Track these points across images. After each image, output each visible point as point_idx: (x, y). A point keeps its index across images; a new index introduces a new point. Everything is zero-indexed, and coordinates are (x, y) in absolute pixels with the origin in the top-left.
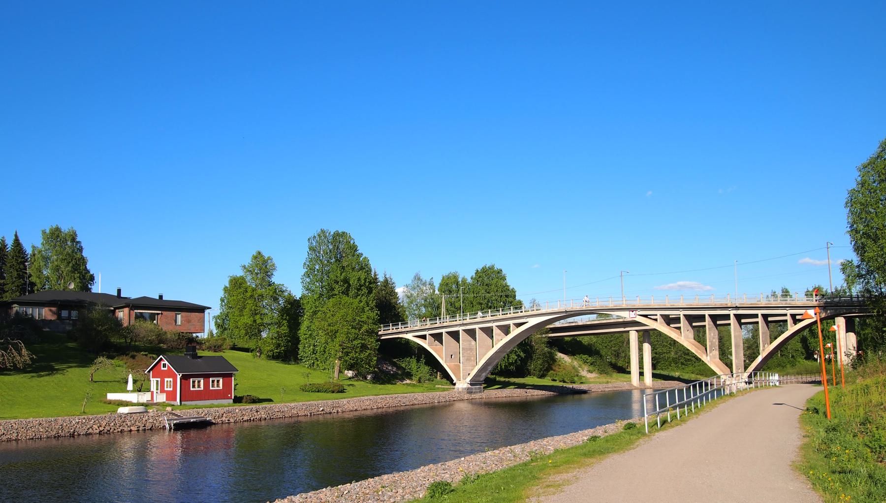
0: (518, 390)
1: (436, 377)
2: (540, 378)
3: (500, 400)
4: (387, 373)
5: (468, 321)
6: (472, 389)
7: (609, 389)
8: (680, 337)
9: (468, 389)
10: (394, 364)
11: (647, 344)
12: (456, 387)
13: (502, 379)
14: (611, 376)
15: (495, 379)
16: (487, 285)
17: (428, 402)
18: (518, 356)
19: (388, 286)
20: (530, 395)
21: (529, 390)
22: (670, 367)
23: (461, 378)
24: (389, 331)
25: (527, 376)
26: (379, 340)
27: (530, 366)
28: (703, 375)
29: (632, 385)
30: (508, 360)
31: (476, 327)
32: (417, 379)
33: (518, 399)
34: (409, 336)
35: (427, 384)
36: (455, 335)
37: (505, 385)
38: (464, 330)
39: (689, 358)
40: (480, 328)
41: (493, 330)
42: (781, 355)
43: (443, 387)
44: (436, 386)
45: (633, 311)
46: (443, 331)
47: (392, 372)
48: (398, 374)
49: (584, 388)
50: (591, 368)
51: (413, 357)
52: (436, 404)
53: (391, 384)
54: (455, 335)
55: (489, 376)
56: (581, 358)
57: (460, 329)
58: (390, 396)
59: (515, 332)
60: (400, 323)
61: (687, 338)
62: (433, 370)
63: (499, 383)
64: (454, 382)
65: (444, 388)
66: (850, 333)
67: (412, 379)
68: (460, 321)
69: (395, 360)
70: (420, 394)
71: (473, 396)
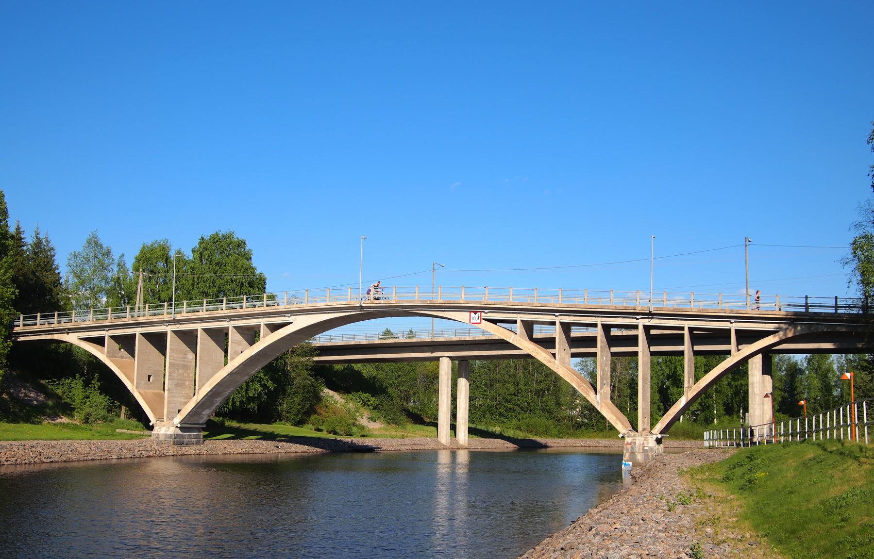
0: (264, 442)
1: (119, 416)
2: (295, 425)
3: (232, 458)
4: (24, 404)
5: (184, 315)
6: (182, 436)
7: (407, 448)
9: (176, 436)
10: (42, 389)
11: (464, 379)
12: (154, 432)
13: (235, 424)
14: (404, 427)
15: (223, 423)
16: (217, 264)
17: (99, 458)
18: (265, 387)
19: (41, 250)
20: (282, 451)
21: (281, 444)
22: (483, 419)
23: (165, 418)
24: (35, 327)
25: (275, 421)
26: (16, 343)
27: (281, 404)
28: (532, 432)
29: (439, 442)
30: (246, 393)
31: (199, 326)
32: (82, 416)
33: (259, 457)
34: (72, 338)
35: (100, 426)
36: (158, 341)
37: (240, 434)
38: (174, 332)
39: (510, 406)
40: (206, 330)
41: (227, 334)
43: (129, 432)
44: (117, 430)
45: (475, 313)
46: (137, 331)
47: (35, 402)
48: (46, 406)
49: (370, 444)
50: (375, 414)
51: (78, 376)
52: (114, 461)
53: (31, 423)
54: (158, 341)
55: (212, 418)
56: (360, 397)
57: (169, 329)
58: (23, 442)
59: (267, 339)
60: (56, 313)
61: (563, 363)
62: (113, 403)
63: (230, 430)
64: (151, 424)
65: (131, 434)
66: (765, 375)
67: (74, 417)
68: (169, 316)
69: (43, 382)
70: (83, 442)
71: (185, 450)
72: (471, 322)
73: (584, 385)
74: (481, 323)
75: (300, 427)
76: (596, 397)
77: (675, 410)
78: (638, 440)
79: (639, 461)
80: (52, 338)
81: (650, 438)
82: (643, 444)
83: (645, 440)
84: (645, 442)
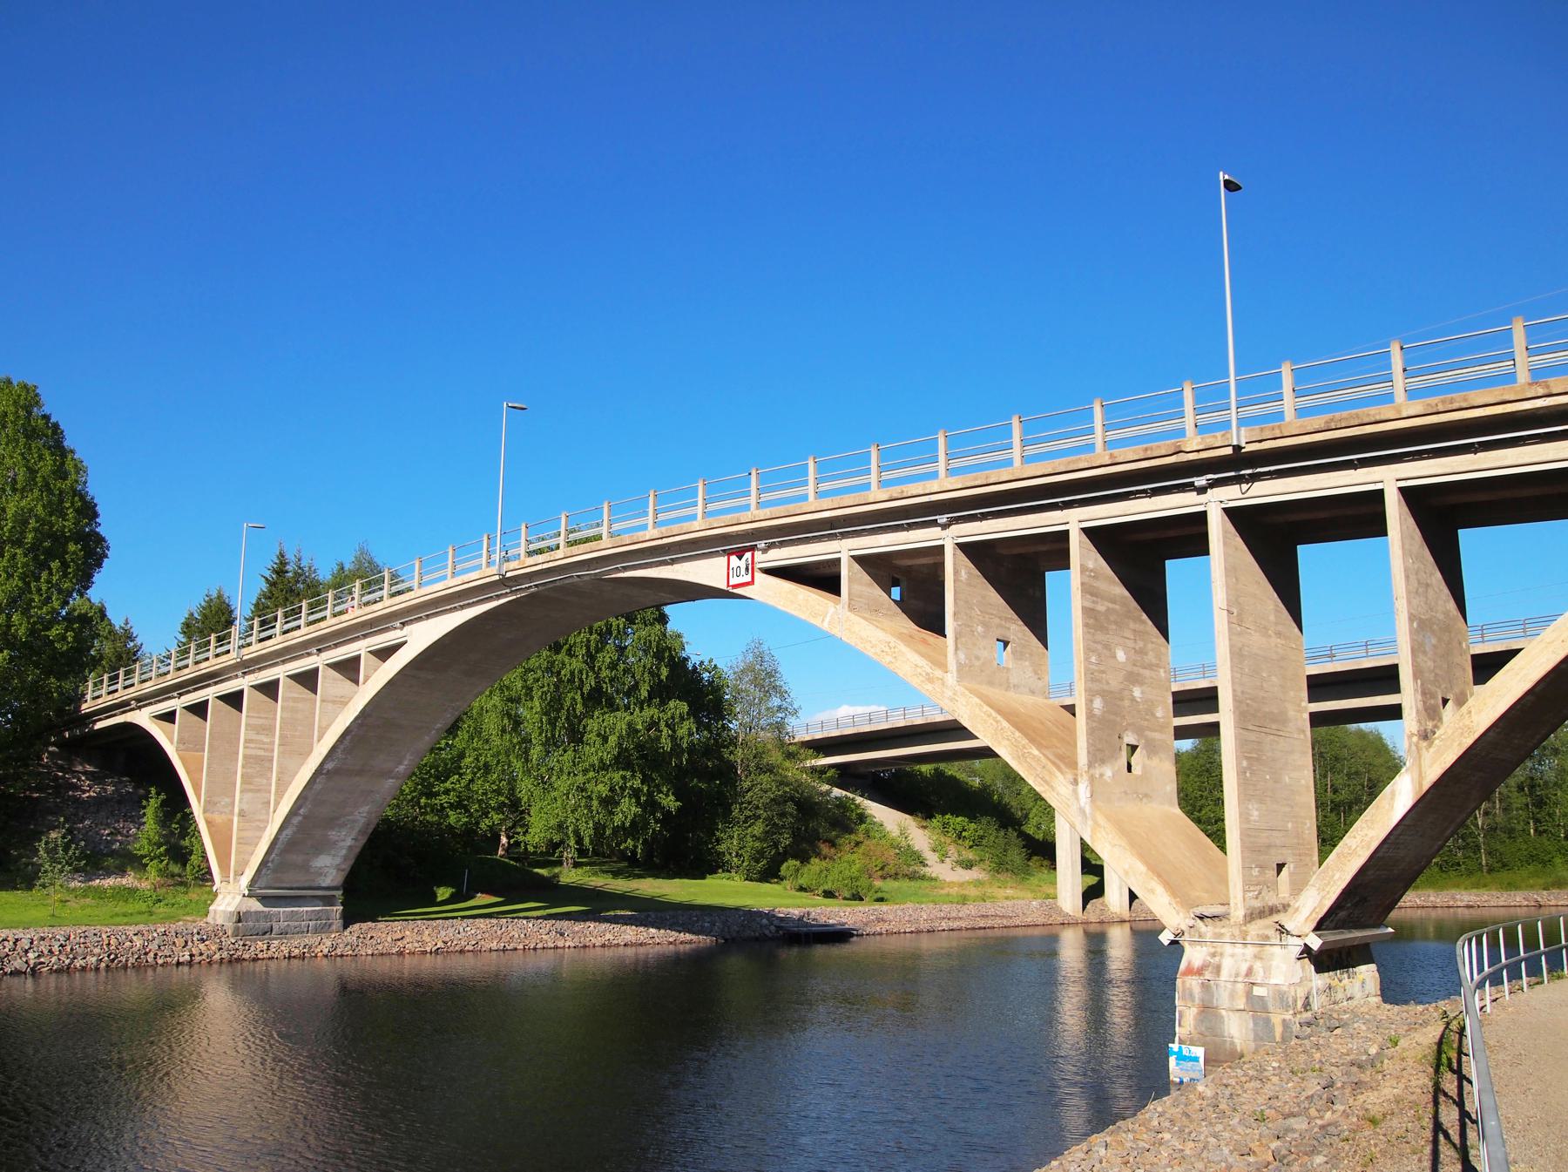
6: (267, 917)
8: (938, 673)
42: (1536, 830)
50: (970, 855)
72: (731, 584)
73: (1036, 752)
74: (752, 582)
75: (775, 883)
76: (1075, 792)
77: (1371, 833)
78: (1233, 956)
79: (1232, 1043)
80: (129, 720)
81: (1277, 950)
82: (1249, 972)
83: (1257, 957)
84: (1258, 966)
